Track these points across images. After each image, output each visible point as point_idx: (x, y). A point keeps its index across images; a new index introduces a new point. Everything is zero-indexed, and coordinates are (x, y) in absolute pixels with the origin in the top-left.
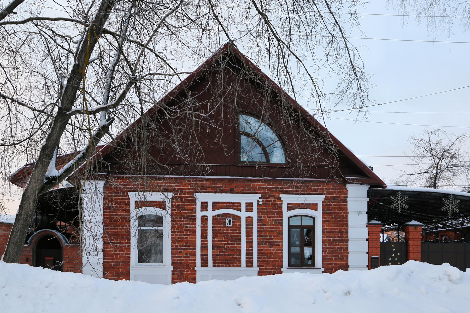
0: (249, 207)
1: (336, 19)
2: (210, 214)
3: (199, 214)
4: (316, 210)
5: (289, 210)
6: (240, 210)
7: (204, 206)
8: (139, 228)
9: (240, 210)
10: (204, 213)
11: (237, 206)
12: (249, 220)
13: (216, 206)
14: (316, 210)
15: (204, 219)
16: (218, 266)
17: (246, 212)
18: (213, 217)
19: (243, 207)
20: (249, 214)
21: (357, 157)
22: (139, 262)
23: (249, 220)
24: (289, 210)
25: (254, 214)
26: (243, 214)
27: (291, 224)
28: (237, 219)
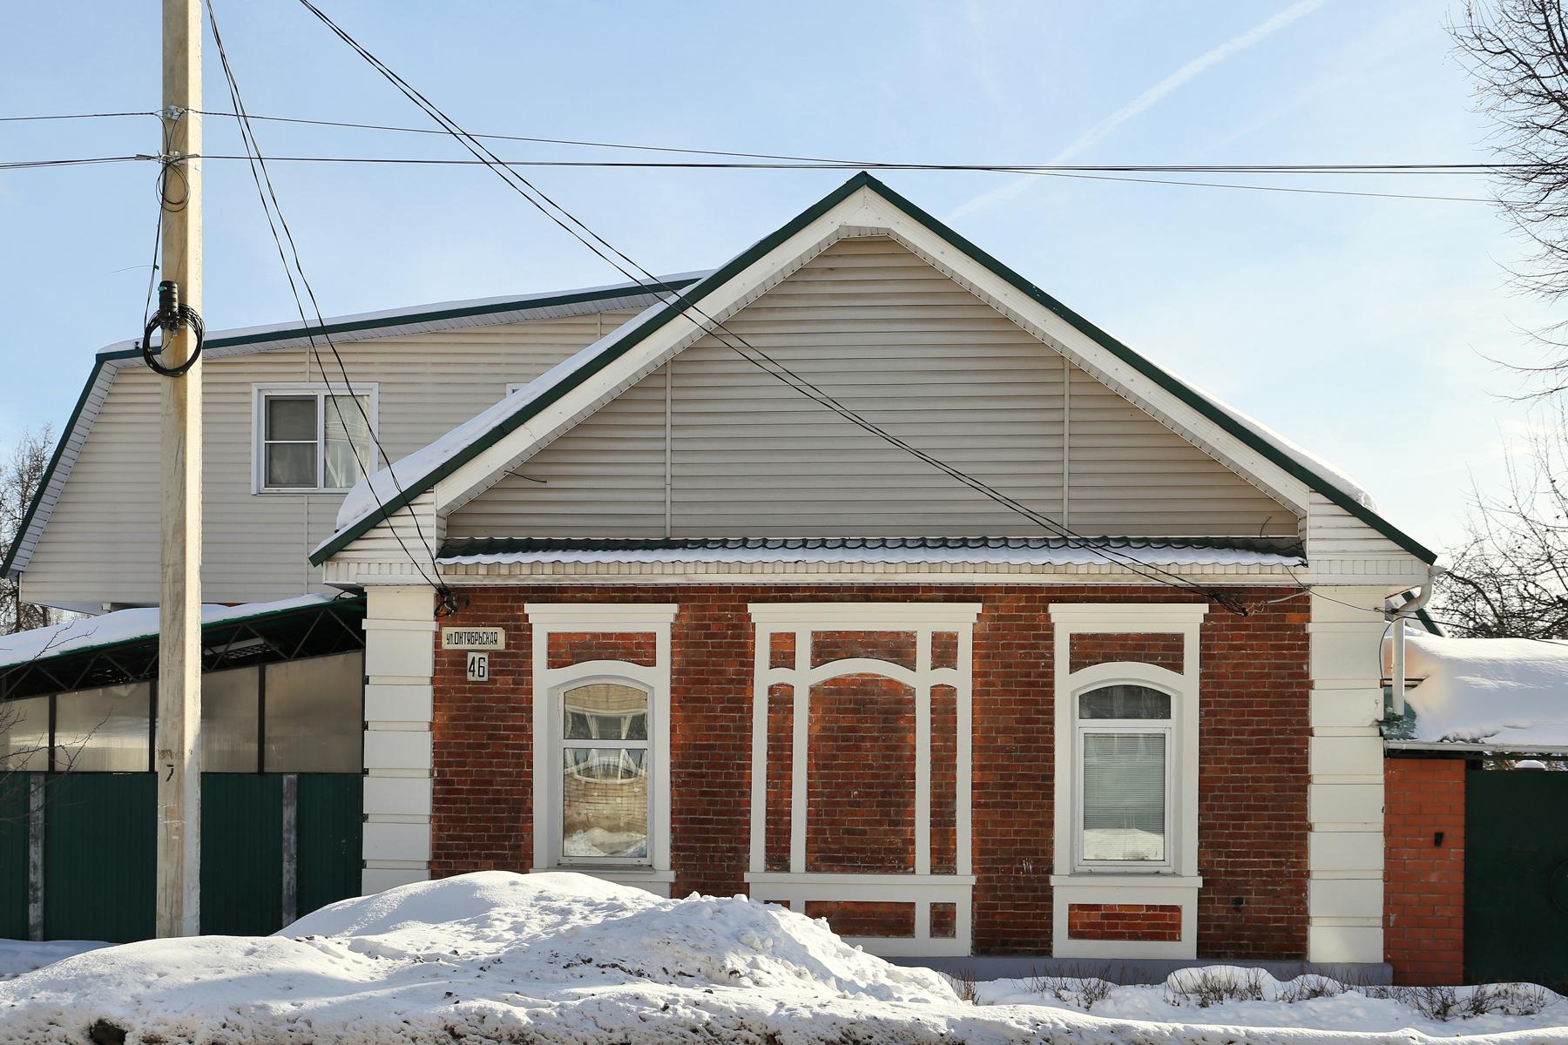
0: (944, 650)
1: (333, 337)
2: (804, 677)
3: (764, 677)
4: (1177, 667)
5: (1075, 666)
6: (911, 665)
7: (783, 655)
8: (624, 737)
9: (911, 665)
10: (782, 675)
11: (898, 648)
12: (943, 700)
13: (828, 647)
14: (1177, 667)
15: (781, 700)
16: (937, 874)
17: (771, 668)
18: (812, 690)
19: (922, 919)
20: (944, 676)
21: (44, 655)
22: (806, 902)
23: (943, 700)
24: (555, 662)
25: (961, 677)
26: (921, 679)
27: (145, 687)
28: (898, 704)
